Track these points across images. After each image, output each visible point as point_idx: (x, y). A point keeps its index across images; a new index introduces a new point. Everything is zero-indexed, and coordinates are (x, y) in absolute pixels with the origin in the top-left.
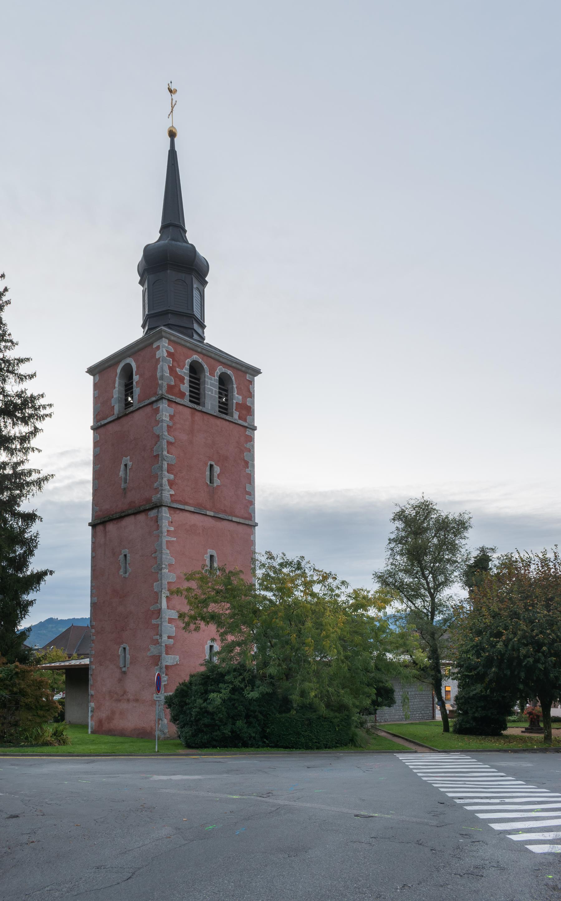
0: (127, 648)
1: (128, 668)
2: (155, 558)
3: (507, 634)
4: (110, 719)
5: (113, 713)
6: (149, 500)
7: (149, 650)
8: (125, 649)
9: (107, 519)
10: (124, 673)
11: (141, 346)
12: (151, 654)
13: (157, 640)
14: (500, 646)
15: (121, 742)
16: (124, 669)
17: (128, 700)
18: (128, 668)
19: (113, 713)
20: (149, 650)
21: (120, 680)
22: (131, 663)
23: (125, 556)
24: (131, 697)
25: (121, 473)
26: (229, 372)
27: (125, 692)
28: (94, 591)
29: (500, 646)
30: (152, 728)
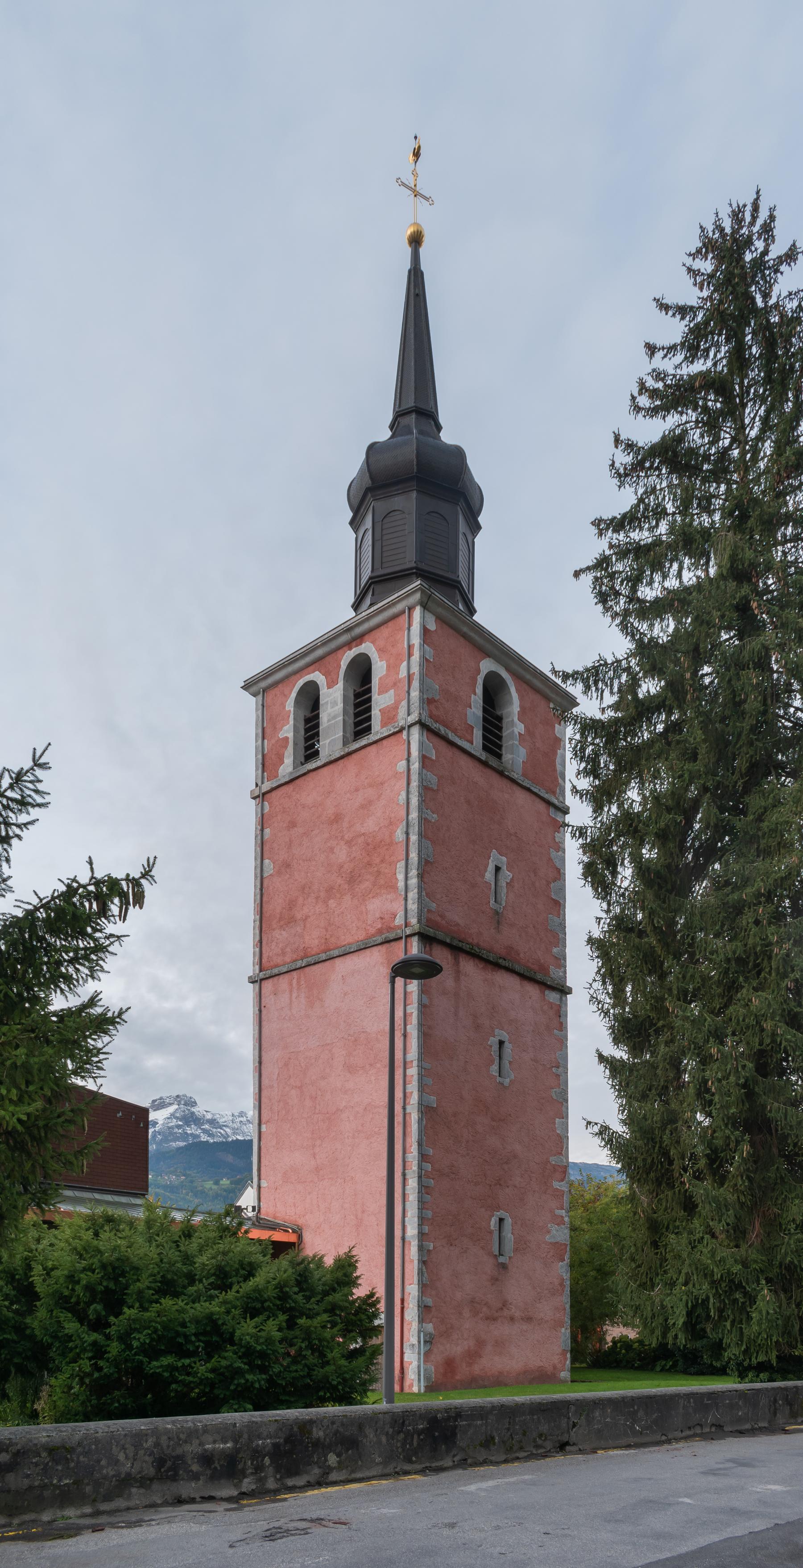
0: (508, 1222)
1: (510, 1258)
2: (558, 1076)
3: (662, 1280)
4: (473, 1355)
5: (480, 1343)
6: (545, 970)
7: (549, 1232)
8: (501, 1220)
9: (467, 947)
10: (504, 1266)
11: (537, 683)
12: (553, 1240)
13: (562, 1217)
14: (114, 1348)
15: (67, 1529)
16: (501, 1260)
17: (512, 1319)
18: (510, 1258)
19: (480, 1343)
20: (549, 1232)
21: (495, 1280)
22: (516, 1250)
23: (501, 1043)
24: (518, 1314)
25: (489, 875)
26: (505, 674)
27: (505, 1304)
28: (429, 1081)
29: (114, 1348)
30: (555, 1367)
